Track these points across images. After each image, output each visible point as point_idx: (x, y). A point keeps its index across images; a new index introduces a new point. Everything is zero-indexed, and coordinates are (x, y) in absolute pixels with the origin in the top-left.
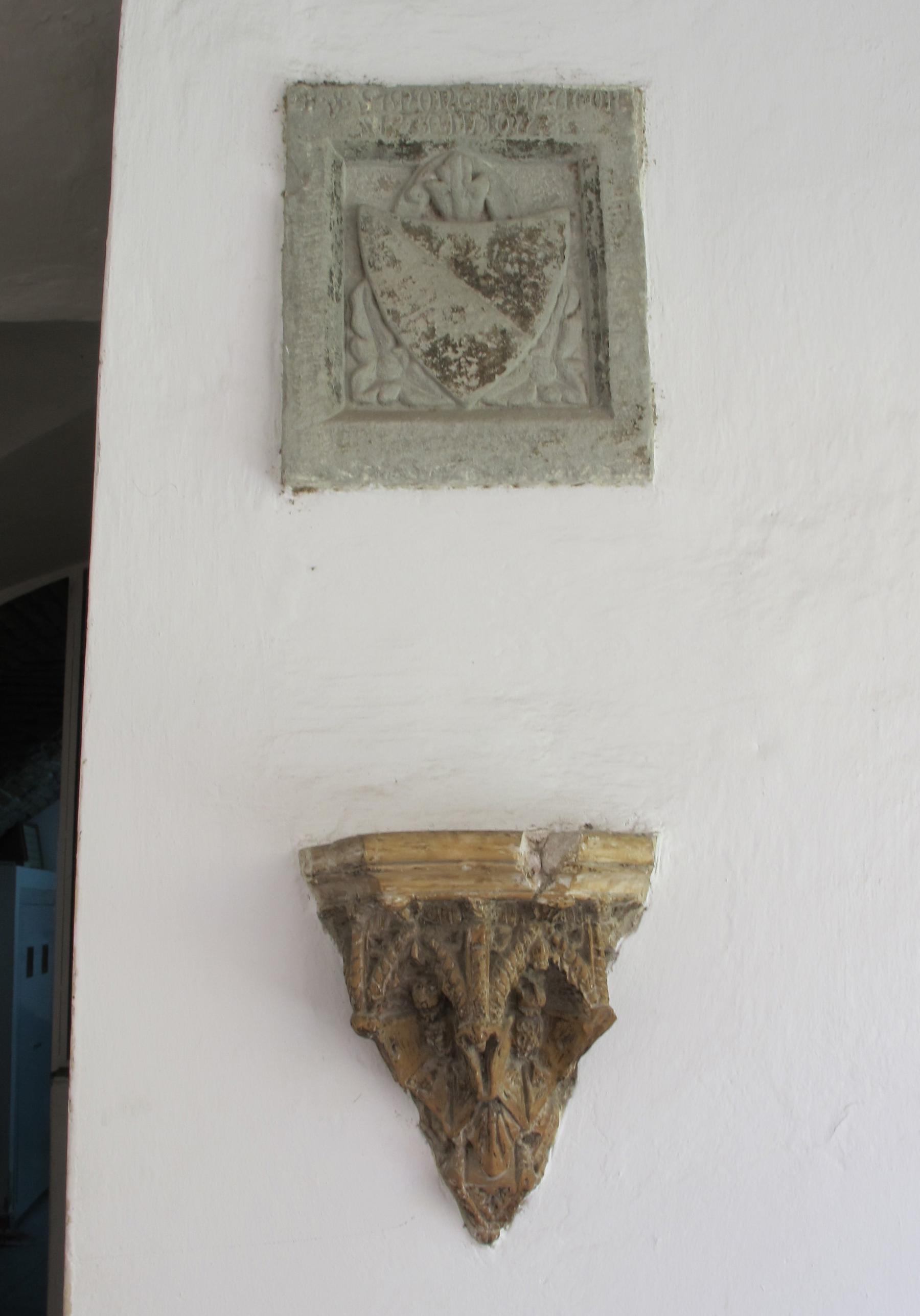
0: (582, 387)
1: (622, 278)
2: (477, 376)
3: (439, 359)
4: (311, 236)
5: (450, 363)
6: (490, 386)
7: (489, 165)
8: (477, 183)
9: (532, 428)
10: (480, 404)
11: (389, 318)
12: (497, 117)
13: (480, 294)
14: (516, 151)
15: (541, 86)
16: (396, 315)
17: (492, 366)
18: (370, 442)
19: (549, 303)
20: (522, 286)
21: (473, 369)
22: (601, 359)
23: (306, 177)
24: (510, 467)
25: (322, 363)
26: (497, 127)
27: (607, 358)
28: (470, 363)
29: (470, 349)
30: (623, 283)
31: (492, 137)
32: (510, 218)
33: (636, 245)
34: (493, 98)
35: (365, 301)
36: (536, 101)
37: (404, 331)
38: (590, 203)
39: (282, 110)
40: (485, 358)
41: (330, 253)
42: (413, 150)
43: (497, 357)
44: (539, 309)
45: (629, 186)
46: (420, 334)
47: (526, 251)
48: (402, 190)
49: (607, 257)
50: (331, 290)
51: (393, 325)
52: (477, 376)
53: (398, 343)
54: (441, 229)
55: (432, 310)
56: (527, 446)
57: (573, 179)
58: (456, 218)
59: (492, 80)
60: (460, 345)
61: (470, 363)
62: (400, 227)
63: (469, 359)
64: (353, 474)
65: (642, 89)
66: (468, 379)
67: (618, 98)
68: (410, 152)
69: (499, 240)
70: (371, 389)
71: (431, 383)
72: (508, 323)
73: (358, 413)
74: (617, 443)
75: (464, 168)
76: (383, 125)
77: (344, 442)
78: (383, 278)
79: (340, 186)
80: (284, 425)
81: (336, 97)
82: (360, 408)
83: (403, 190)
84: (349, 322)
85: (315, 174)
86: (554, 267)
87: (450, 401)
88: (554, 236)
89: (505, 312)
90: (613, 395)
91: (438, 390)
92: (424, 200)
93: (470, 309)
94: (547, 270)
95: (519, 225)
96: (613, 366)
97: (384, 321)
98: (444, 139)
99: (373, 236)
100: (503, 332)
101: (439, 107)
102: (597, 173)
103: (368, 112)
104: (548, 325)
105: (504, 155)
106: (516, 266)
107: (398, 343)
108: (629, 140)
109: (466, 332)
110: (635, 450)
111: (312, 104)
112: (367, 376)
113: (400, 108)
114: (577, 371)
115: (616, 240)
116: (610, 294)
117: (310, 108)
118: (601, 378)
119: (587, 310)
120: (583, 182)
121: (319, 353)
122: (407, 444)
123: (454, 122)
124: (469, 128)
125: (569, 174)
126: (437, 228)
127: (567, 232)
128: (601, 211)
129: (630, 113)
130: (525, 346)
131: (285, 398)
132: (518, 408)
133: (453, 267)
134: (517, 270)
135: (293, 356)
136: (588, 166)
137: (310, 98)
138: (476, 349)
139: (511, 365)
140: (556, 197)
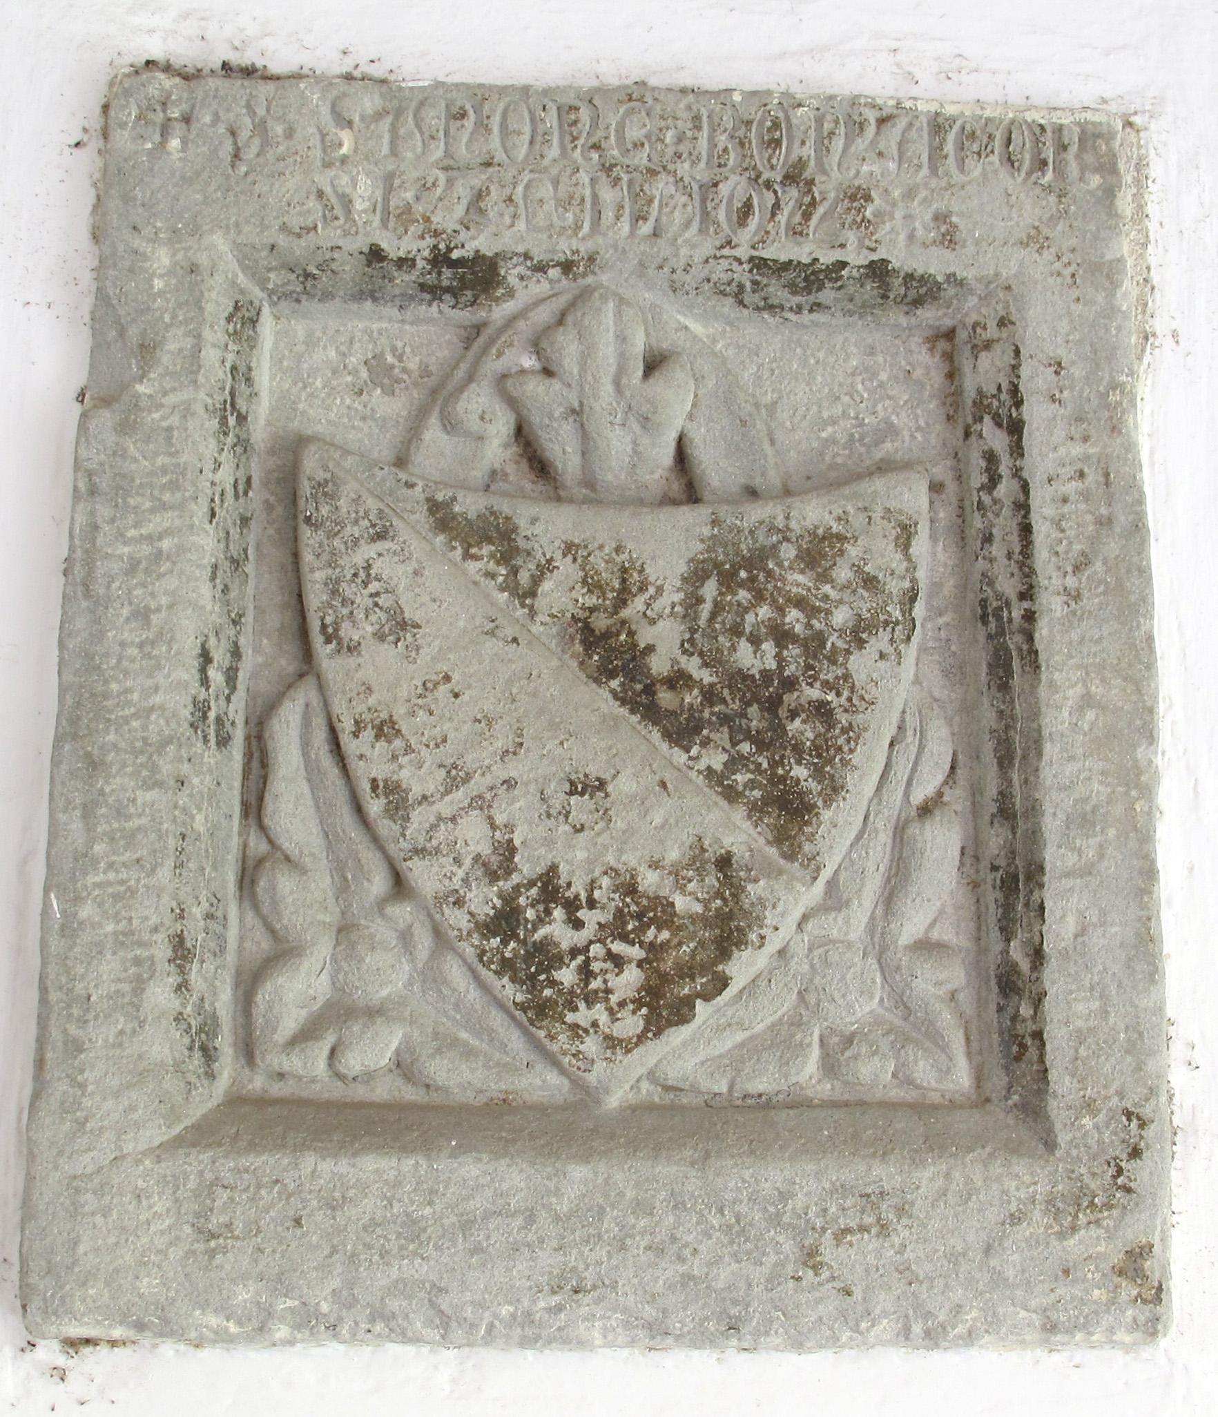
0: (957, 1040)
1: (1088, 700)
2: (639, 1003)
3: (522, 947)
4: (149, 538)
5: (558, 961)
6: (677, 1036)
7: (696, 328)
8: (657, 385)
9: (806, 1182)
10: (645, 1086)
11: (375, 807)
12: (724, 189)
13: (656, 735)
14: (777, 291)
15: (854, 101)
16: (398, 800)
17: (687, 971)
18: (298, 1222)
19: (866, 764)
20: (783, 713)
21: (629, 980)
22: (1017, 953)
23: (147, 351)
24: (734, 1311)
25: (162, 951)
26: (721, 215)
27: (1038, 956)
28: (618, 962)
29: (620, 914)
30: (1090, 715)
31: (707, 247)
32: (752, 493)
33: (1128, 594)
34: (713, 130)
35: (305, 745)
36: (838, 144)
37: (419, 852)
38: (991, 458)
39: (96, 143)
40: (665, 946)
41: (205, 592)
42: (473, 278)
43: (701, 943)
44: (834, 789)
45: (1106, 414)
46: (468, 862)
47: (800, 603)
48: (434, 392)
49: (1042, 631)
50: (201, 709)
51: (386, 828)
52: (639, 1003)
53: (399, 885)
54: (545, 526)
55: (509, 783)
56: (788, 1246)
57: (937, 379)
58: (592, 492)
59: (712, 79)
60: (592, 904)
61: (618, 962)
62: (421, 516)
63: (617, 947)
64: (240, 1323)
65: (1137, 120)
66: (611, 1011)
67: (1074, 148)
68: (464, 285)
69: (717, 565)
70: (306, 1035)
71: (497, 1020)
72: (739, 833)
73: (267, 1120)
74: (1061, 1236)
75: (622, 339)
76: (386, 200)
77: (215, 1222)
78: (370, 673)
79: (249, 380)
80: (31, 1157)
81: (251, 112)
82: (278, 1090)
83: (438, 396)
84: (254, 808)
85: (175, 343)
86: (882, 656)
87: (553, 1078)
88: (882, 555)
89: (731, 794)
90: (1053, 1075)
91: (516, 1041)
92: (501, 426)
93: (624, 786)
94: (861, 664)
95: (780, 522)
96: (1054, 979)
97: (359, 810)
98: (565, 247)
99: (337, 542)
100: (724, 862)
101: (554, 152)
102: (1015, 368)
103: (344, 160)
104: (859, 837)
105: (739, 298)
106: (768, 647)
107: (399, 885)
108: (1107, 273)
109: (611, 860)
110: (1117, 1258)
111: (179, 128)
112: (296, 992)
113: (438, 152)
114: (943, 985)
115: (1071, 581)
116: (1049, 749)
117: (174, 143)
118: (1015, 1018)
119: (975, 791)
120: (970, 394)
121: (154, 920)
122: (413, 1230)
123: (595, 196)
124: (639, 217)
125: (927, 364)
126: (534, 521)
127: (921, 546)
128: (1025, 487)
129: (1110, 193)
130: (786, 907)
131: (40, 1064)
132: (764, 1104)
133: (579, 648)
134: (772, 664)
135: (70, 928)
136: (988, 345)
137: (175, 113)
138: (639, 916)
139: (742, 968)
140: (890, 430)
